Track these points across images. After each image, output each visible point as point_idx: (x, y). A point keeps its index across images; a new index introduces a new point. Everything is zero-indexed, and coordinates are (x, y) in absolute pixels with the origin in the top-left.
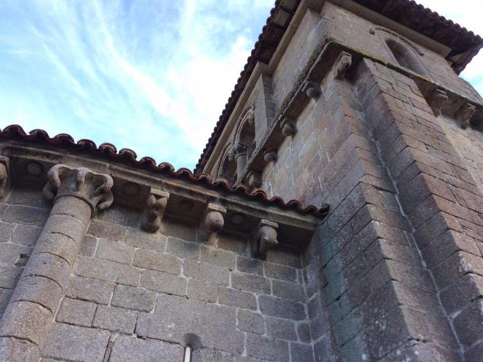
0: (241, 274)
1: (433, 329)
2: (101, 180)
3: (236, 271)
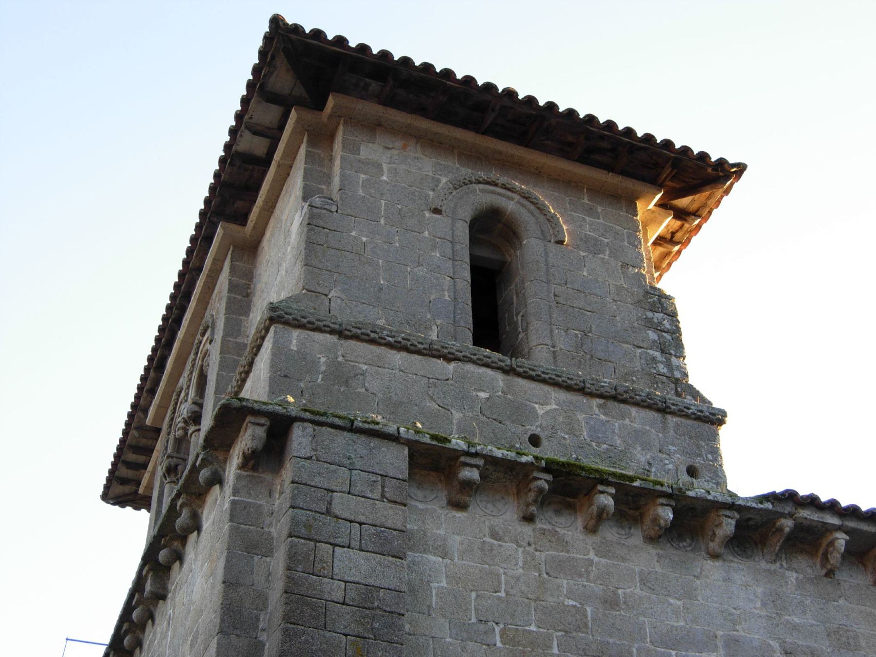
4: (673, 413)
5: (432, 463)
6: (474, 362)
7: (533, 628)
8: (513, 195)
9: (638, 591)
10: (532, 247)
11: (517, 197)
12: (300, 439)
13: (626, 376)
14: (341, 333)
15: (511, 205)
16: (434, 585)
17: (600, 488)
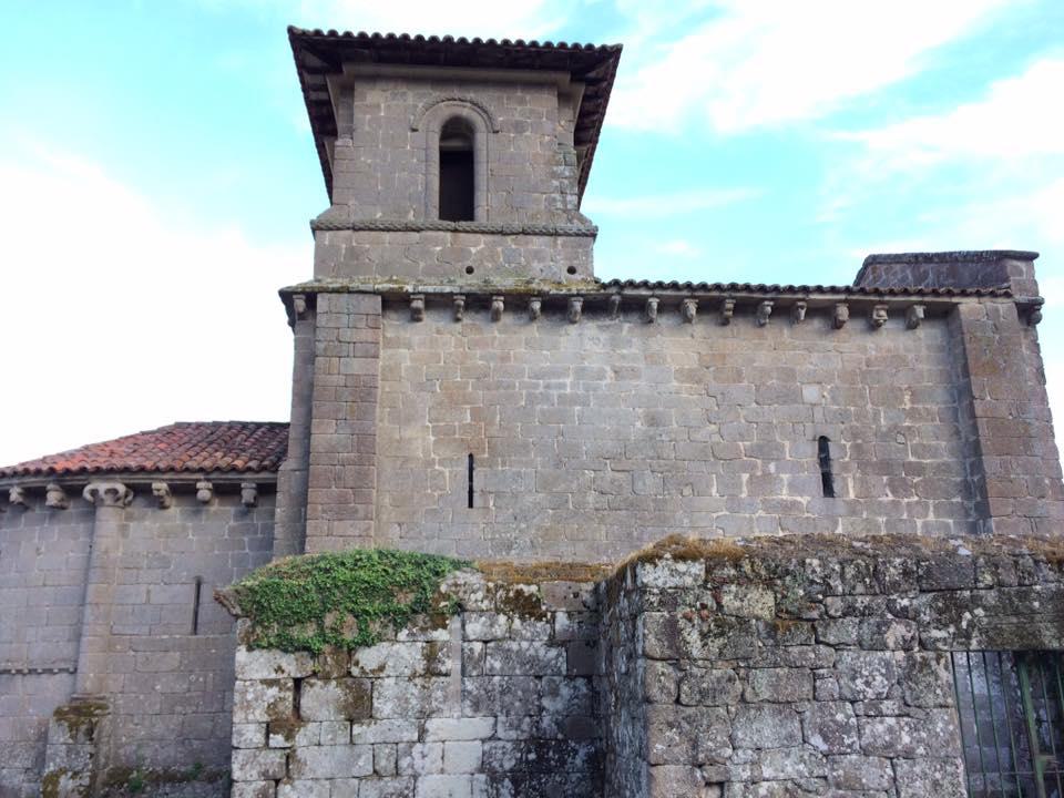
0: (235, 524)
1: (621, 318)
2: (115, 492)
3: (232, 523)
4: (560, 235)
5: (395, 302)
6: (431, 229)
7: (459, 379)
8: (465, 104)
9: (523, 350)
10: (482, 141)
11: (469, 105)
12: (322, 302)
13: (533, 217)
14: (355, 229)
15: (466, 111)
16: (403, 365)
17: (494, 298)
